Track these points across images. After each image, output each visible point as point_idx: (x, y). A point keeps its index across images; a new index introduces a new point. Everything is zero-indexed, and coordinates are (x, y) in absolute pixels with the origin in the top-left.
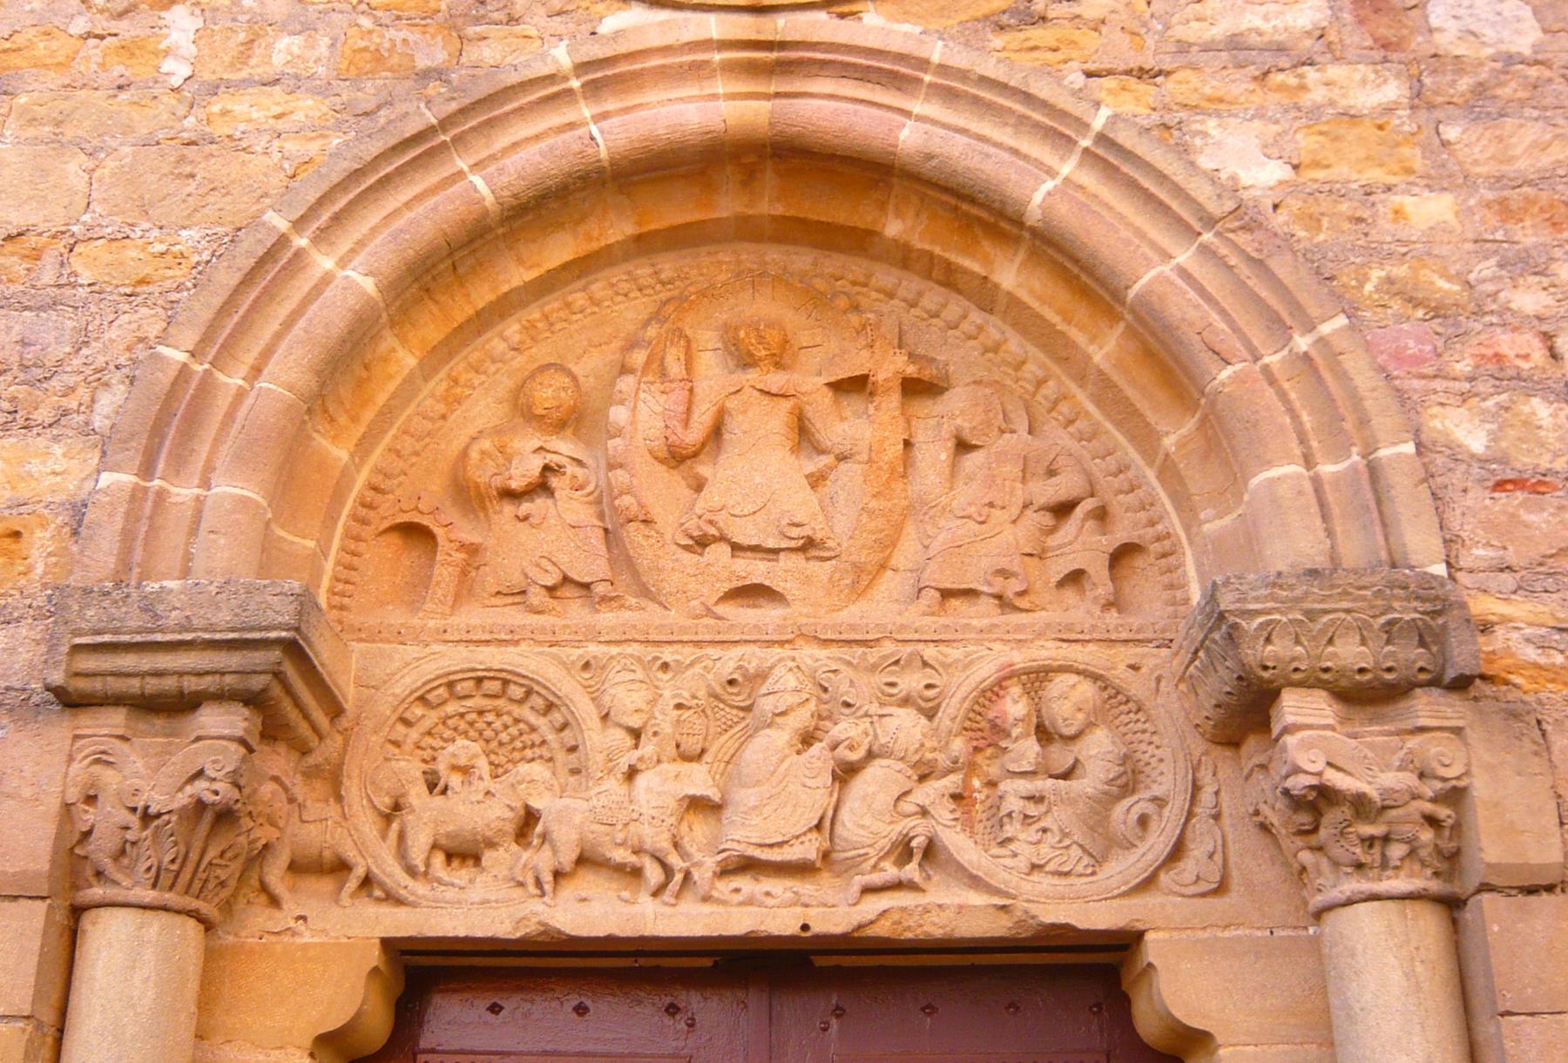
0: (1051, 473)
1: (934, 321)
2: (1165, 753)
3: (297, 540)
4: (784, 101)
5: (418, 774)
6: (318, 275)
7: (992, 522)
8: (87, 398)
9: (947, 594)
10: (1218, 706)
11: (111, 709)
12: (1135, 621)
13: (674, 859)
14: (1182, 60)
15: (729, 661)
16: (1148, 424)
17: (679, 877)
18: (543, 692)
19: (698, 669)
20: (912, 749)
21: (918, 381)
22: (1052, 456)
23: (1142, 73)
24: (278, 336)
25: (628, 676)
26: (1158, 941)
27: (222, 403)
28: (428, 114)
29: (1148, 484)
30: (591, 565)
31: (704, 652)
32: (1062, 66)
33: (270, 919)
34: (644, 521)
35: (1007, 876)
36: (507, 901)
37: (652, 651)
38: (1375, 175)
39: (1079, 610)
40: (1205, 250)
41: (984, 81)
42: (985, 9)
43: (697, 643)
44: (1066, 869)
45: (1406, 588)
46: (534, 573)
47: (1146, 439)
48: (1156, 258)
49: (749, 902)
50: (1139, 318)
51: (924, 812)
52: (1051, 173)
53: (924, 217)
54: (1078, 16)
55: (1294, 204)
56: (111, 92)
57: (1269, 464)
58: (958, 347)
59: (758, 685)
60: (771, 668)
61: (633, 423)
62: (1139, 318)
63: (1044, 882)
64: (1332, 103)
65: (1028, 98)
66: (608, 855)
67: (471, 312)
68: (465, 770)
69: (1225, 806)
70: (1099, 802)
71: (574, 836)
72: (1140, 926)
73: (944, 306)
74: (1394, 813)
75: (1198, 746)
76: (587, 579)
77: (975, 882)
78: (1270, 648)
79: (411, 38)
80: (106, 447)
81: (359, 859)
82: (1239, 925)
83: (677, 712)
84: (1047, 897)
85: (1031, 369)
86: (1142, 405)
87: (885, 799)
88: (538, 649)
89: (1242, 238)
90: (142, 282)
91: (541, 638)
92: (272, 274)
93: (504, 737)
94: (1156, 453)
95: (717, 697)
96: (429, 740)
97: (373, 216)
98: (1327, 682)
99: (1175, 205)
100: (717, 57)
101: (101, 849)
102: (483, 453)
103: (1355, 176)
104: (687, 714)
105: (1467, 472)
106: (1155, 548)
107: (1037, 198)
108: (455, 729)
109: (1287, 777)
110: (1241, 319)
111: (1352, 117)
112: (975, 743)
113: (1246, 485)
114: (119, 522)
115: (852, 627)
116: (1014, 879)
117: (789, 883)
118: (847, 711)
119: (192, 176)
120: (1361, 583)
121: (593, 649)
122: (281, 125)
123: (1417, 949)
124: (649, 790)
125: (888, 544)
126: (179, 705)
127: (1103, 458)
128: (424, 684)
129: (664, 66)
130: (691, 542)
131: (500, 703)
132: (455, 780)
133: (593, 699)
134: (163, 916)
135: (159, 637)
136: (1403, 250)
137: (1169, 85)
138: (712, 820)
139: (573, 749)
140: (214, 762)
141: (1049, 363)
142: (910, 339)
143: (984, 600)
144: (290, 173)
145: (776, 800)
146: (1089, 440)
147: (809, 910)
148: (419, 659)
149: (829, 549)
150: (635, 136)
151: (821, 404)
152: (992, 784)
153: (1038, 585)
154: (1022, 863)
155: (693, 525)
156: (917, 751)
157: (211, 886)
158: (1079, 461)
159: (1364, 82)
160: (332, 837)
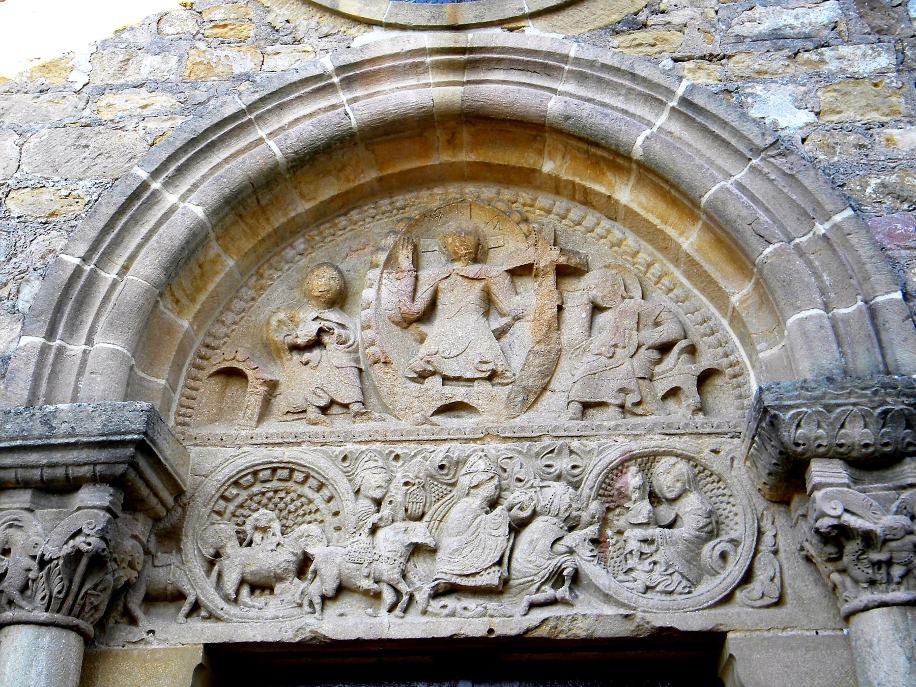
0: (657, 324)
1: (578, 227)
4: (472, 86)
5: (233, 533)
6: (168, 206)
7: (617, 356)
8: (14, 291)
10: (770, 474)
11: (22, 492)
12: (715, 421)
13: (403, 587)
15: (439, 453)
17: (405, 598)
18: (317, 476)
19: (419, 458)
20: (563, 509)
21: (567, 267)
22: (657, 313)
23: (710, 58)
24: (140, 246)
25: (375, 464)
26: (736, 639)
27: (103, 289)
28: (240, 102)
29: (724, 329)
30: (348, 393)
31: (423, 447)
32: (657, 56)
33: (130, 633)
34: (384, 363)
35: (630, 595)
36: (290, 617)
37: (389, 447)
38: (875, 116)
40: (754, 169)
41: (604, 67)
42: (606, 21)
44: (671, 589)
45: (895, 388)
47: (719, 297)
48: (720, 177)
49: (453, 614)
50: (710, 217)
52: (650, 125)
53: (568, 157)
54: (669, 23)
55: (815, 137)
56: (36, 95)
57: (799, 309)
58: (594, 244)
59: (412, 455)
60: (468, 457)
61: (378, 299)
62: (710, 217)
63: (654, 599)
64: (842, 71)
65: (634, 76)
67: (270, 230)
69: (781, 545)
70: (693, 543)
71: (335, 572)
72: (723, 628)
73: (584, 217)
74: (894, 544)
75: (760, 504)
76: (346, 402)
79: (230, 55)
80: (26, 321)
81: (192, 591)
82: (793, 627)
84: (657, 608)
85: (643, 257)
86: (715, 275)
88: (312, 448)
89: (779, 161)
90: (52, 214)
91: (316, 440)
92: (137, 206)
93: (292, 507)
94: (727, 307)
95: (432, 477)
96: (240, 511)
97: (204, 168)
98: (842, 454)
99: (733, 142)
100: (429, 60)
102: (279, 321)
106: (729, 371)
107: (640, 141)
108: (259, 503)
109: (816, 520)
110: (779, 213)
111: (856, 79)
114: (31, 369)
115: (523, 429)
117: (480, 601)
119: (87, 146)
121: (350, 447)
122: (145, 112)
124: (386, 539)
125: (549, 373)
127: (693, 313)
129: (393, 66)
130: (415, 376)
131: (289, 484)
132: (257, 537)
133: (350, 481)
134: (54, 631)
135: (53, 441)
136: (893, 164)
137: (731, 64)
138: (429, 561)
139: (336, 514)
141: (655, 252)
142: (562, 240)
144: (150, 143)
145: (467, 542)
146: (683, 302)
147: (493, 619)
149: (507, 378)
150: (374, 112)
151: (500, 287)
152: (620, 533)
154: (640, 585)
156: (566, 510)
157: (87, 609)
158: (676, 316)
159: (864, 55)
160: (174, 575)
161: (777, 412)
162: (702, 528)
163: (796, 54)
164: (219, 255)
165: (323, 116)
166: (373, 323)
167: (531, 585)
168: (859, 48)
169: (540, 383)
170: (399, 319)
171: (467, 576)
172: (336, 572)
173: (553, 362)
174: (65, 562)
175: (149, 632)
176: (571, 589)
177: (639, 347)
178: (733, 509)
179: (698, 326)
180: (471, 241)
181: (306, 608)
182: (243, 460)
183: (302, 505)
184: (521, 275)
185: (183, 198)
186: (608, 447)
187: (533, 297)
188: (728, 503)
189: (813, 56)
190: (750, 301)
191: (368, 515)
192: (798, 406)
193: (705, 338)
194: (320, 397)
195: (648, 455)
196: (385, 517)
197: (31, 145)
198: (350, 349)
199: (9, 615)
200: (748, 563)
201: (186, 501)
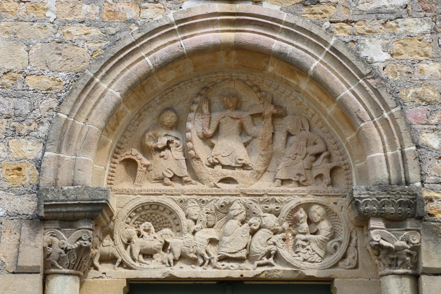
0: (315, 144)
2: (343, 228)
3: (99, 167)
6: (103, 90)
7: (297, 158)
13: (206, 256)
14: (360, 17)
15: (222, 200)
16: (342, 133)
17: (207, 261)
18: (169, 209)
19: (212, 202)
22: (315, 139)
23: (347, 22)
25: (194, 204)
28: (132, 37)
29: (343, 147)
37: (200, 197)
38: (417, 57)
39: (322, 187)
43: (212, 195)
46: (166, 174)
49: (227, 268)
51: (275, 244)
55: (389, 69)
63: (307, 264)
66: (188, 255)
68: (147, 231)
72: (333, 277)
74: (399, 252)
76: (181, 176)
77: (288, 264)
78: (367, 207)
81: (120, 257)
82: (360, 277)
84: (308, 268)
87: (264, 240)
89: (371, 81)
93: (158, 220)
97: (118, 71)
101: (53, 259)
102: (149, 136)
103: (410, 58)
104: (209, 215)
106: (344, 167)
108: (144, 218)
112: (290, 224)
113: (366, 158)
115: (256, 191)
116: (298, 263)
118: (254, 215)
121: (183, 197)
127: (331, 139)
128: (136, 207)
131: (157, 211)
133: (183, 211)
135: (69, 202)
143: (293, 182)
144: (91, 54)
147: (243, 271)
148: (134, 199)
149: (250, 167)
150: (194, 46)
151: (247, 122)
153: (309, 178)
154: (301, 259)
155: (211, 159)
161: (358, 200)
162: (328, 235)
163: (386, 22)
164: (124, 108)
168: (415, 20)
171: (233, 253)
176: (274, 258)
178: (341, 227)
179: (332, 145)
182: (138, 201)
183: (163, 220)
184: (256, 116)
185: (109, 86)
188: (339, 225)
189: (393, 24)
190: (354, 141)
192: (367, 198)
193: (335, 151)
194: (169, 173)
197: (33, 51)
199: (53, 270)
200: (345, 251)
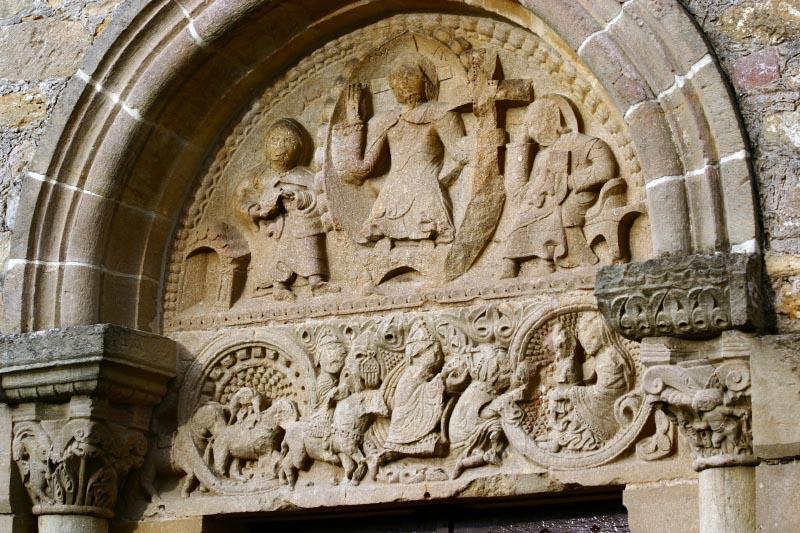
0: (589, 162)
1: (519, 51)
7: (547, 204)
9: (256, 422)
11: (28, 405)
15: (384, 323)
19: (367, 330)
20: (490, 374)
37: (342, 322)
43: (368, 313)
49: (397, 481)
72: (621, 482)
73: (523, 40)
83: (359, 360)
88: (278, 326)
90: (22, 122)
91: (279, 318)
95: (382, 347)
97: (137, 61)
105: (787, 164)
115: (457, 293)
120: (678, 268)
121: (309, 322)
123: (729, 499)
124: (341, 413)
126: (62, 399)
135: (38, 365)
140: (79, 432)
154: (553, 445)
156: (493, 375)
162: (611, 384)
165: (71, 234)
166: (324, 188)
167: (463, 450)
169: (482, 236)
170: (351, 178)
171: (409, 444)
172: (301, 446)
173: (496, 210)
174: (68, 467)
175: (160, 507)
177: (569, 191)
180: (414, 80)
181: (281, 480)
183: (279, 379)
186: (534, 306)
187: (472, 145)
191: (326, 389)
192: (623, 292)
195: (570, 312)
196: (341, 391)
198: (312, 213)
201: (177, 386)
